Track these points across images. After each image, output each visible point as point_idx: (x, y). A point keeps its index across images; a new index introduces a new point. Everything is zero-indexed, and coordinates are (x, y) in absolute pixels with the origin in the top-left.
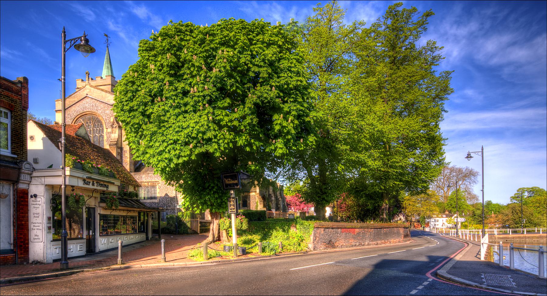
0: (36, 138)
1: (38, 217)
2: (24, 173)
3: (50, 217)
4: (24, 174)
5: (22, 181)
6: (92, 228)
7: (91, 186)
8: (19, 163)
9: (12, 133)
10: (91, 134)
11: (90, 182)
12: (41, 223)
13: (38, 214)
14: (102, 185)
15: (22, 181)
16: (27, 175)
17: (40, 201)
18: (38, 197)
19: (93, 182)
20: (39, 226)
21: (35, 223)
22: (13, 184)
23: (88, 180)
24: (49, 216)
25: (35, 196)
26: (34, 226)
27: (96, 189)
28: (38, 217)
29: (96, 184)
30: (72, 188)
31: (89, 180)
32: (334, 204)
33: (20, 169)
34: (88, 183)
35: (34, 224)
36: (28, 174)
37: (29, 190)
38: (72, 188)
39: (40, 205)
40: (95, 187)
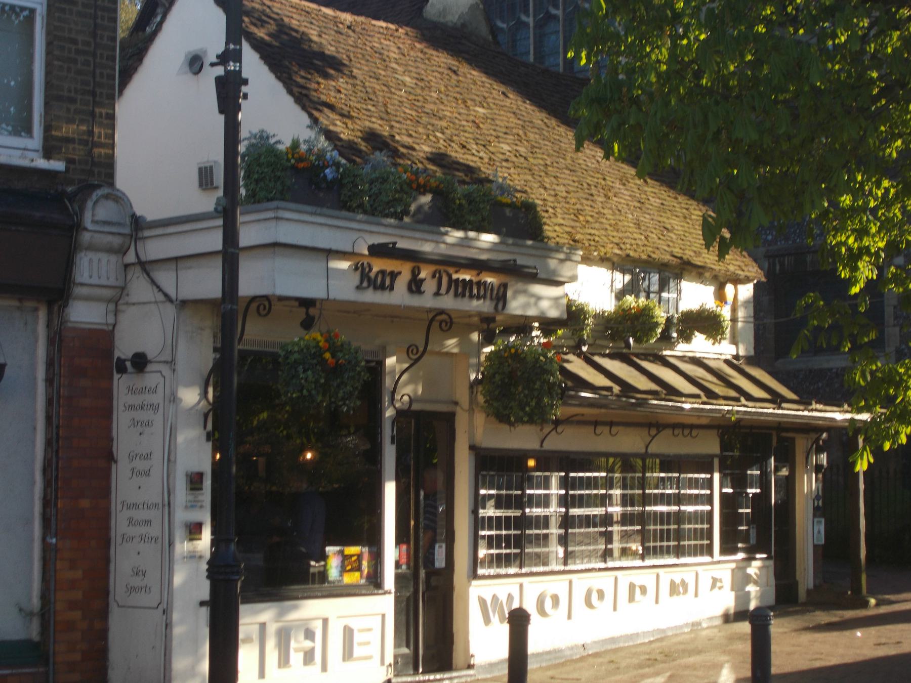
0: (180, 59)
1: (147, 474)
2: (91, 248)
3: (200, 475)
4: (91, 255)
5: (84, 291)
6: (442, 532)
7: (399, 296)
8: (72, 197)
9: (48, 52)
10: (527, 13)
11: (394, 275)
12: (156, 505)
13: (148, 457)
14: (467, 284)
15: (84, 291)
16: (104, 257)
17: (155, 391)
18: (149, 368)
19: (415, 273)
20: (148, 522)
21: (135, 506)
22: (50, 305)
23: (378, 265)
24: (196, 469)
25: (140, 362)
26: (130, 520)
27: (441, 312)
28: (147, 474)
29: (429, 286)
30: (301, 313)
31: (389, 265)
32: (788, 486)
33: (77, 227)
34: (384, 283)
35: (133, 513)
36: (110, 250)
37: (118, 335)
38: (301, 313)
39: (154, 408)
40: (427, 301)
